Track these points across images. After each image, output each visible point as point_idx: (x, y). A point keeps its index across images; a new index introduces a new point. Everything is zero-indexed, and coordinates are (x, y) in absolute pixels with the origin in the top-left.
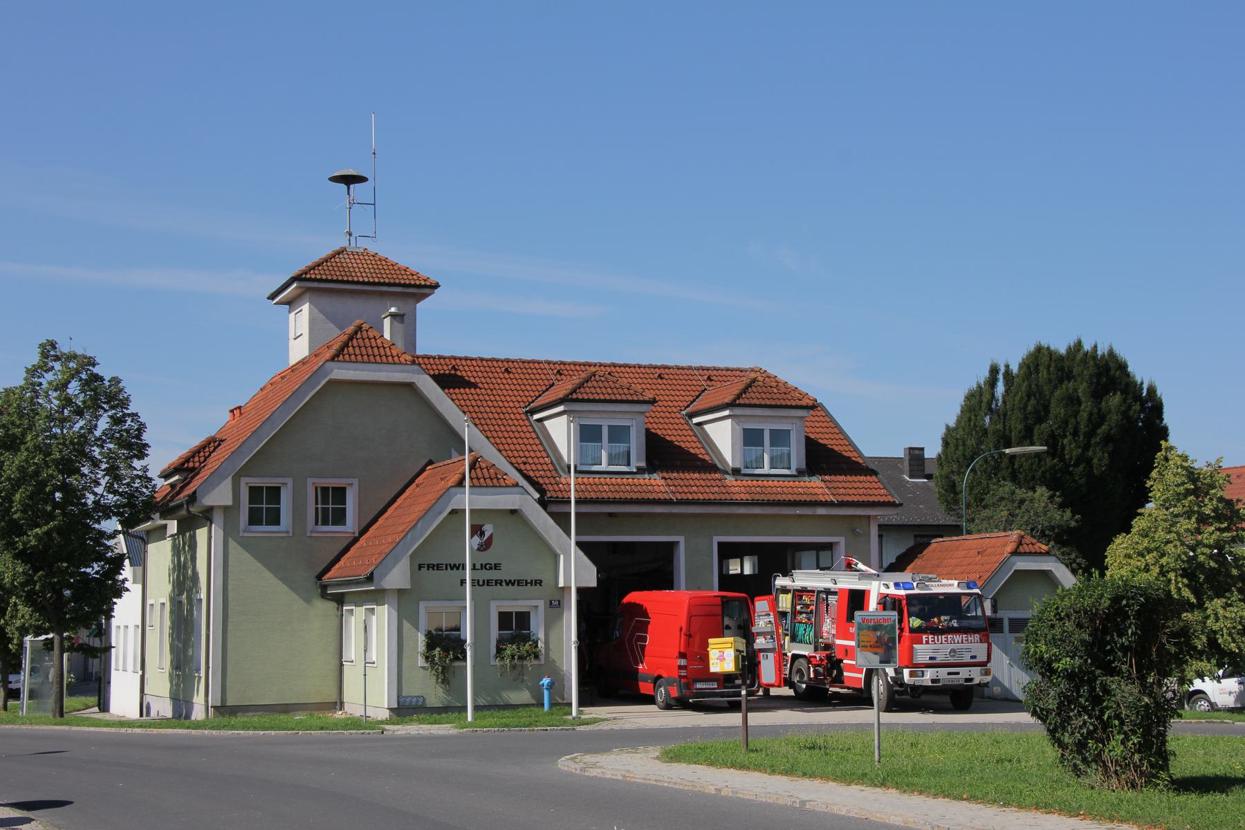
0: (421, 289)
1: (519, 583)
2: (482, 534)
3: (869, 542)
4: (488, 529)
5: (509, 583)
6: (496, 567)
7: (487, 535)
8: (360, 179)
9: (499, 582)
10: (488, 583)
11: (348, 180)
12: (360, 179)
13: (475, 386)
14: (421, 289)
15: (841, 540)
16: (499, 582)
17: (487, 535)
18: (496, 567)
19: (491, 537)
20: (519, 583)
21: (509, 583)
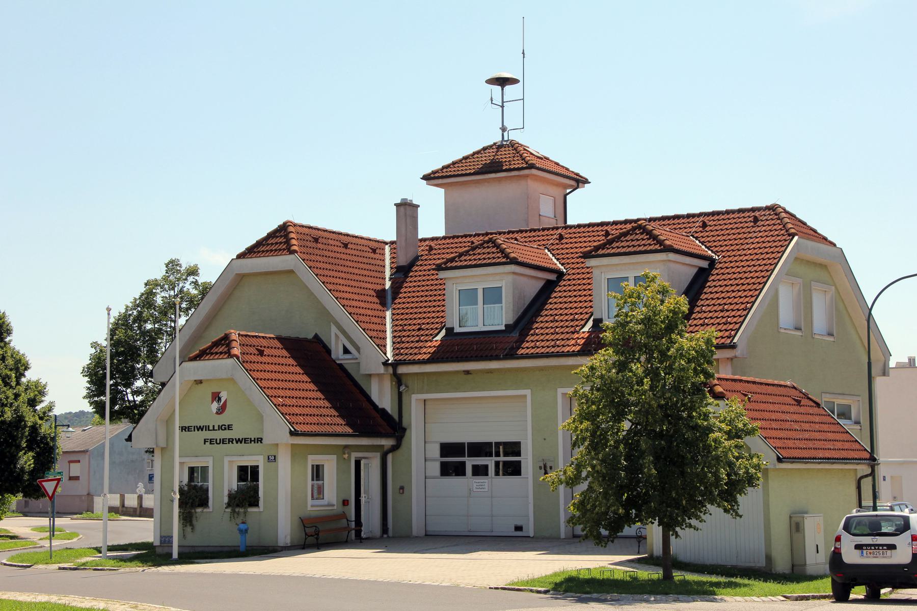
0: (579, 181)
1: (245, 441)
2: (220, 399)
3: (103, 459)
4: (224, 396)
5: (239, 441)
6: (229, 427)
7: (223, 400)
8: (513, 81)
9: (231, 441)
10: (223, 441)
11: (502, 82)
12: (513, 81)
13: (417, 258)
14: (579, 181)
15: (528, 392)
16: (231, 441)
17: (223, 400)
18: (229, 427)
19: (226, 401)
20: (245, 441)
21: (239, 441)
